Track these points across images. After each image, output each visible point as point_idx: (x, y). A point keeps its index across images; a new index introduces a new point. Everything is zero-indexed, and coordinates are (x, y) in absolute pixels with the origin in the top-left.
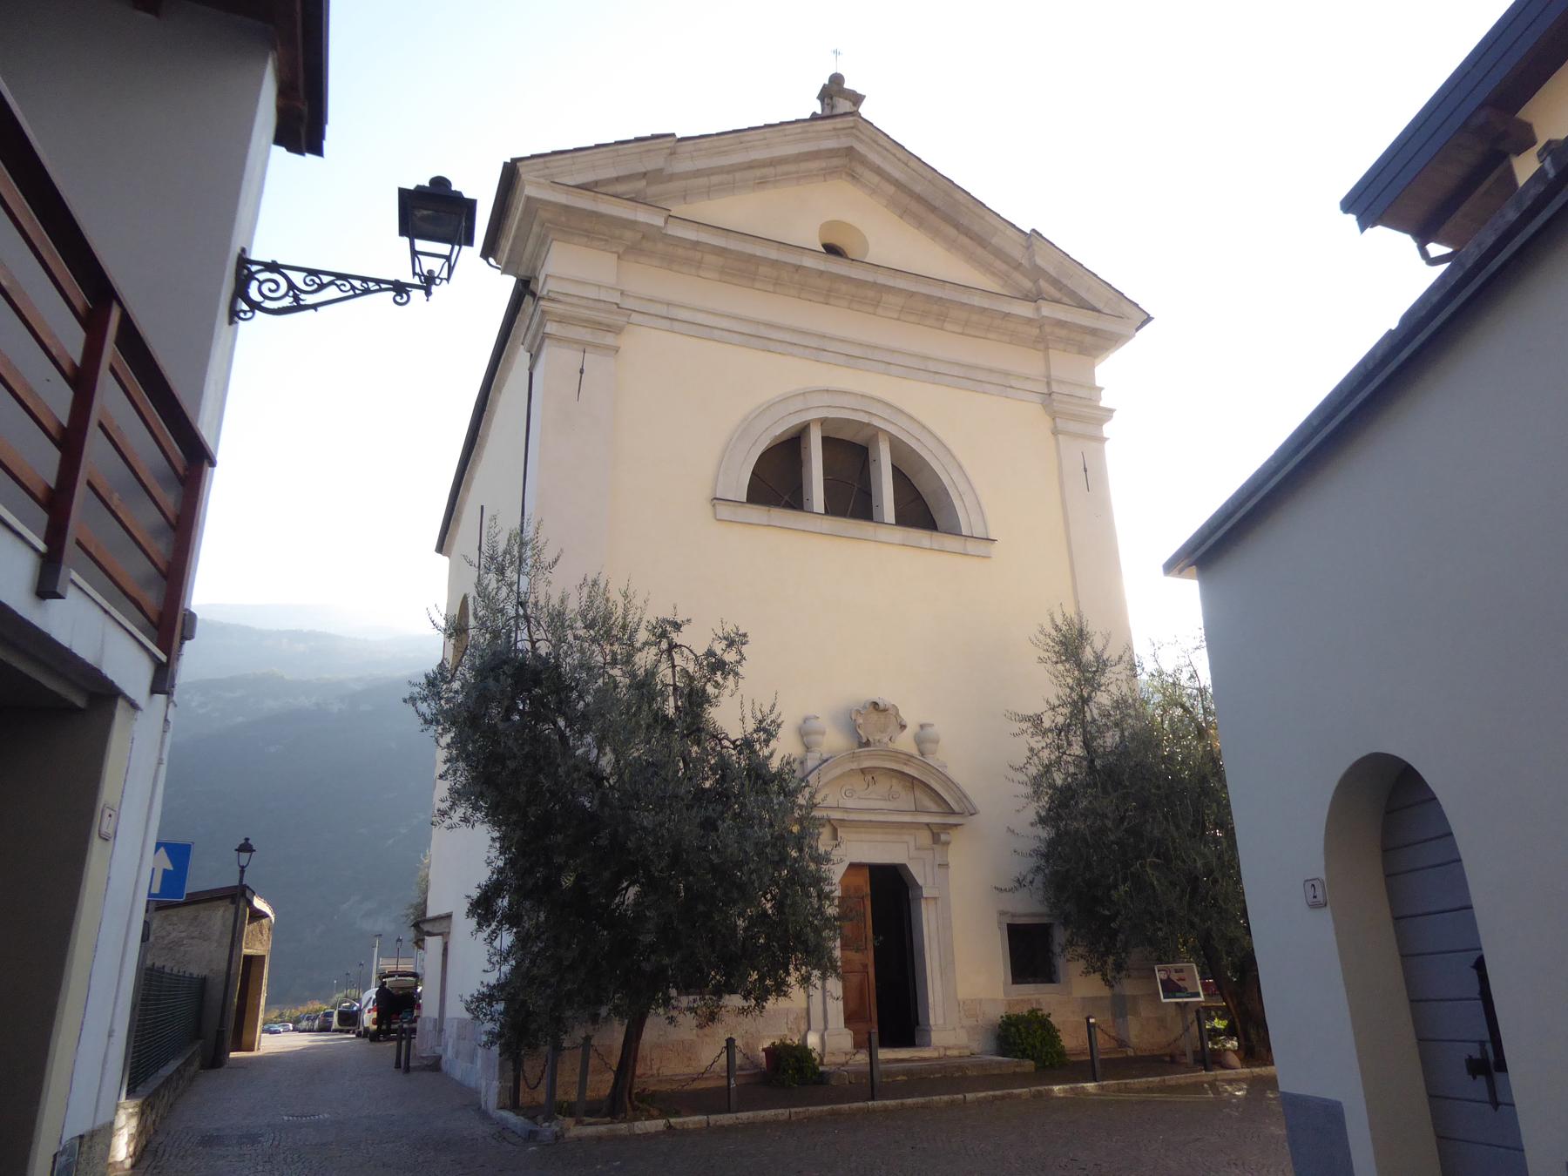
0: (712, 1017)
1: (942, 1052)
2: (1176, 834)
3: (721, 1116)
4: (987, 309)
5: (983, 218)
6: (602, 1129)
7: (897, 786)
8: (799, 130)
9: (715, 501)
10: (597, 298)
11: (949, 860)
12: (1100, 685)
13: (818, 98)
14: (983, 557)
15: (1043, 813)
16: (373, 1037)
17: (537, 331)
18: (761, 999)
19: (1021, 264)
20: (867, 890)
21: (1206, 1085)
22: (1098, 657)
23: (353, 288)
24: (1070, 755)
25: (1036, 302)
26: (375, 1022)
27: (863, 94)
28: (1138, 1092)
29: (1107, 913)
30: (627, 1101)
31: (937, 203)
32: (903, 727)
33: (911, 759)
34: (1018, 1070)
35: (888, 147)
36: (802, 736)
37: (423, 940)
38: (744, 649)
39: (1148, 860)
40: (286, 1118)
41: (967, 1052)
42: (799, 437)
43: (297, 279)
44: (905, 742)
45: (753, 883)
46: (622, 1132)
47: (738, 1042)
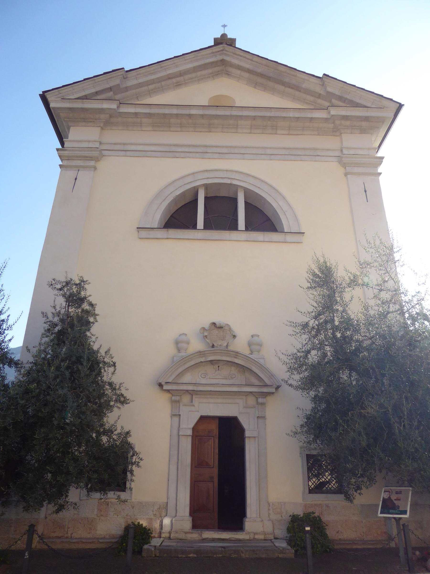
1: (252, 536)
5: (296, 76)
7: (233, 370)
8: (193, 56)
19: (320, 94)
25: (327, 109)
33: (238, 355)
47: (40, 529)
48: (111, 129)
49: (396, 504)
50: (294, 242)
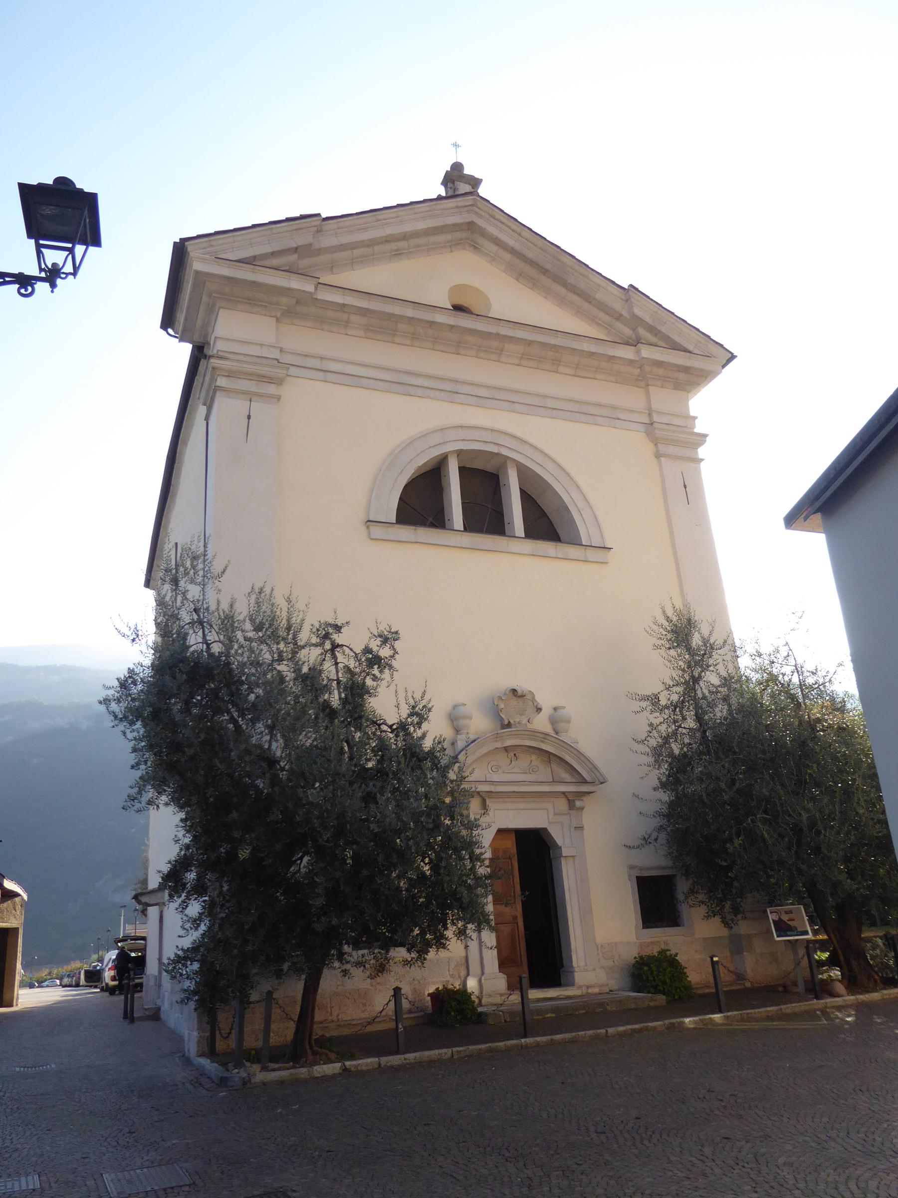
0: (381, 969)
1: (584, 990)
2: (782, 792)
3: (391, 1058)
4: (593, 353)
5: (587, 277)
6: (285, 1074)
7: (535, 760)
8: (428, 209)
9: (369, 523)
12: (708, 666)
13: (442, 183)
14: (601, 563)
15: (664, 779)
16: (111, 991)
17: (210, 385)
18: (422, 952)
19: (621, 315)
20: (514, 850)
21: (818, 1012)
22: (705, 642)
24: (685, 728)
25: (636, 346)
26: (113, 979)
28: (758, 1020)
29: (724, 864)
30: (308, 1047)
31: (548, 266)
32: (539, 710)
34: (652, 1004)
35: (504, 220)
36: (452, 721)
37: (146, 910)
38: (397, 644)
39: (758, 816)
40: (18, 1069)
42: (440, 468)
44: (541, 723)
46: (302, 1076)
49: (792, 925)
50: (597, 562)
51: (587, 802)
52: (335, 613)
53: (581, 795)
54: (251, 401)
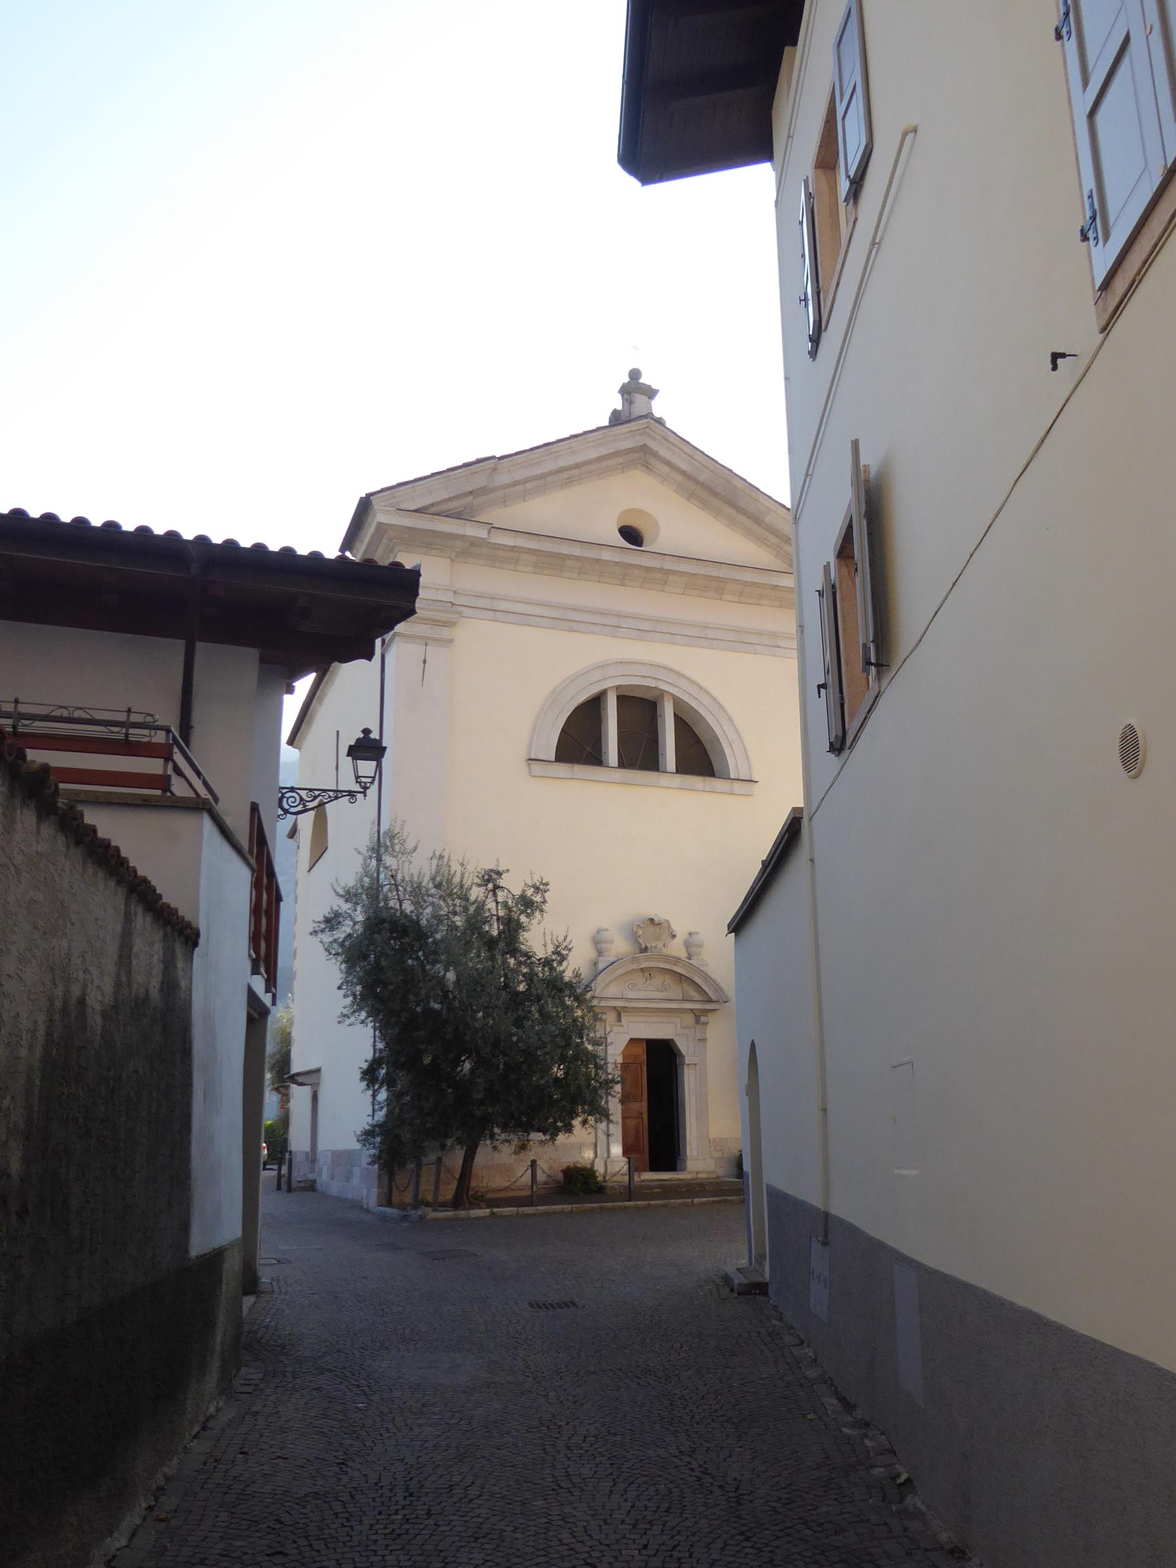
0: (523, 1147)
1: (695, 1176)
7: (668, 979)
8: (600, 437)
9: (530, 762)
10: (435, 598)
11: (707, 1036)
23: (330, 797)
27: (657, 388)
32: (674, 936)
33: (680, 961)
41: (713, 1176)
43: (303, 793)
44: (676, 948)
45: (546, 1061)
48: (466, 563)
51: (711, 1018)
52: (498, 861)
53: (706, 1012)
54: (426, 645)
